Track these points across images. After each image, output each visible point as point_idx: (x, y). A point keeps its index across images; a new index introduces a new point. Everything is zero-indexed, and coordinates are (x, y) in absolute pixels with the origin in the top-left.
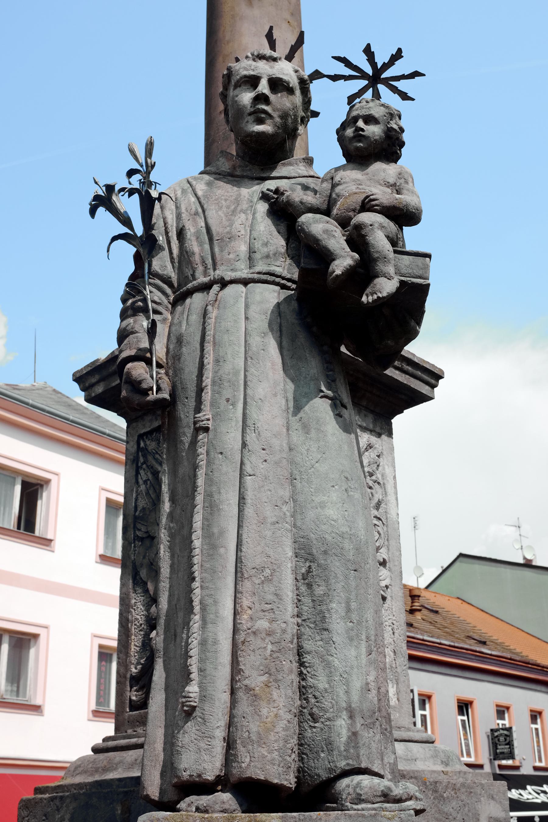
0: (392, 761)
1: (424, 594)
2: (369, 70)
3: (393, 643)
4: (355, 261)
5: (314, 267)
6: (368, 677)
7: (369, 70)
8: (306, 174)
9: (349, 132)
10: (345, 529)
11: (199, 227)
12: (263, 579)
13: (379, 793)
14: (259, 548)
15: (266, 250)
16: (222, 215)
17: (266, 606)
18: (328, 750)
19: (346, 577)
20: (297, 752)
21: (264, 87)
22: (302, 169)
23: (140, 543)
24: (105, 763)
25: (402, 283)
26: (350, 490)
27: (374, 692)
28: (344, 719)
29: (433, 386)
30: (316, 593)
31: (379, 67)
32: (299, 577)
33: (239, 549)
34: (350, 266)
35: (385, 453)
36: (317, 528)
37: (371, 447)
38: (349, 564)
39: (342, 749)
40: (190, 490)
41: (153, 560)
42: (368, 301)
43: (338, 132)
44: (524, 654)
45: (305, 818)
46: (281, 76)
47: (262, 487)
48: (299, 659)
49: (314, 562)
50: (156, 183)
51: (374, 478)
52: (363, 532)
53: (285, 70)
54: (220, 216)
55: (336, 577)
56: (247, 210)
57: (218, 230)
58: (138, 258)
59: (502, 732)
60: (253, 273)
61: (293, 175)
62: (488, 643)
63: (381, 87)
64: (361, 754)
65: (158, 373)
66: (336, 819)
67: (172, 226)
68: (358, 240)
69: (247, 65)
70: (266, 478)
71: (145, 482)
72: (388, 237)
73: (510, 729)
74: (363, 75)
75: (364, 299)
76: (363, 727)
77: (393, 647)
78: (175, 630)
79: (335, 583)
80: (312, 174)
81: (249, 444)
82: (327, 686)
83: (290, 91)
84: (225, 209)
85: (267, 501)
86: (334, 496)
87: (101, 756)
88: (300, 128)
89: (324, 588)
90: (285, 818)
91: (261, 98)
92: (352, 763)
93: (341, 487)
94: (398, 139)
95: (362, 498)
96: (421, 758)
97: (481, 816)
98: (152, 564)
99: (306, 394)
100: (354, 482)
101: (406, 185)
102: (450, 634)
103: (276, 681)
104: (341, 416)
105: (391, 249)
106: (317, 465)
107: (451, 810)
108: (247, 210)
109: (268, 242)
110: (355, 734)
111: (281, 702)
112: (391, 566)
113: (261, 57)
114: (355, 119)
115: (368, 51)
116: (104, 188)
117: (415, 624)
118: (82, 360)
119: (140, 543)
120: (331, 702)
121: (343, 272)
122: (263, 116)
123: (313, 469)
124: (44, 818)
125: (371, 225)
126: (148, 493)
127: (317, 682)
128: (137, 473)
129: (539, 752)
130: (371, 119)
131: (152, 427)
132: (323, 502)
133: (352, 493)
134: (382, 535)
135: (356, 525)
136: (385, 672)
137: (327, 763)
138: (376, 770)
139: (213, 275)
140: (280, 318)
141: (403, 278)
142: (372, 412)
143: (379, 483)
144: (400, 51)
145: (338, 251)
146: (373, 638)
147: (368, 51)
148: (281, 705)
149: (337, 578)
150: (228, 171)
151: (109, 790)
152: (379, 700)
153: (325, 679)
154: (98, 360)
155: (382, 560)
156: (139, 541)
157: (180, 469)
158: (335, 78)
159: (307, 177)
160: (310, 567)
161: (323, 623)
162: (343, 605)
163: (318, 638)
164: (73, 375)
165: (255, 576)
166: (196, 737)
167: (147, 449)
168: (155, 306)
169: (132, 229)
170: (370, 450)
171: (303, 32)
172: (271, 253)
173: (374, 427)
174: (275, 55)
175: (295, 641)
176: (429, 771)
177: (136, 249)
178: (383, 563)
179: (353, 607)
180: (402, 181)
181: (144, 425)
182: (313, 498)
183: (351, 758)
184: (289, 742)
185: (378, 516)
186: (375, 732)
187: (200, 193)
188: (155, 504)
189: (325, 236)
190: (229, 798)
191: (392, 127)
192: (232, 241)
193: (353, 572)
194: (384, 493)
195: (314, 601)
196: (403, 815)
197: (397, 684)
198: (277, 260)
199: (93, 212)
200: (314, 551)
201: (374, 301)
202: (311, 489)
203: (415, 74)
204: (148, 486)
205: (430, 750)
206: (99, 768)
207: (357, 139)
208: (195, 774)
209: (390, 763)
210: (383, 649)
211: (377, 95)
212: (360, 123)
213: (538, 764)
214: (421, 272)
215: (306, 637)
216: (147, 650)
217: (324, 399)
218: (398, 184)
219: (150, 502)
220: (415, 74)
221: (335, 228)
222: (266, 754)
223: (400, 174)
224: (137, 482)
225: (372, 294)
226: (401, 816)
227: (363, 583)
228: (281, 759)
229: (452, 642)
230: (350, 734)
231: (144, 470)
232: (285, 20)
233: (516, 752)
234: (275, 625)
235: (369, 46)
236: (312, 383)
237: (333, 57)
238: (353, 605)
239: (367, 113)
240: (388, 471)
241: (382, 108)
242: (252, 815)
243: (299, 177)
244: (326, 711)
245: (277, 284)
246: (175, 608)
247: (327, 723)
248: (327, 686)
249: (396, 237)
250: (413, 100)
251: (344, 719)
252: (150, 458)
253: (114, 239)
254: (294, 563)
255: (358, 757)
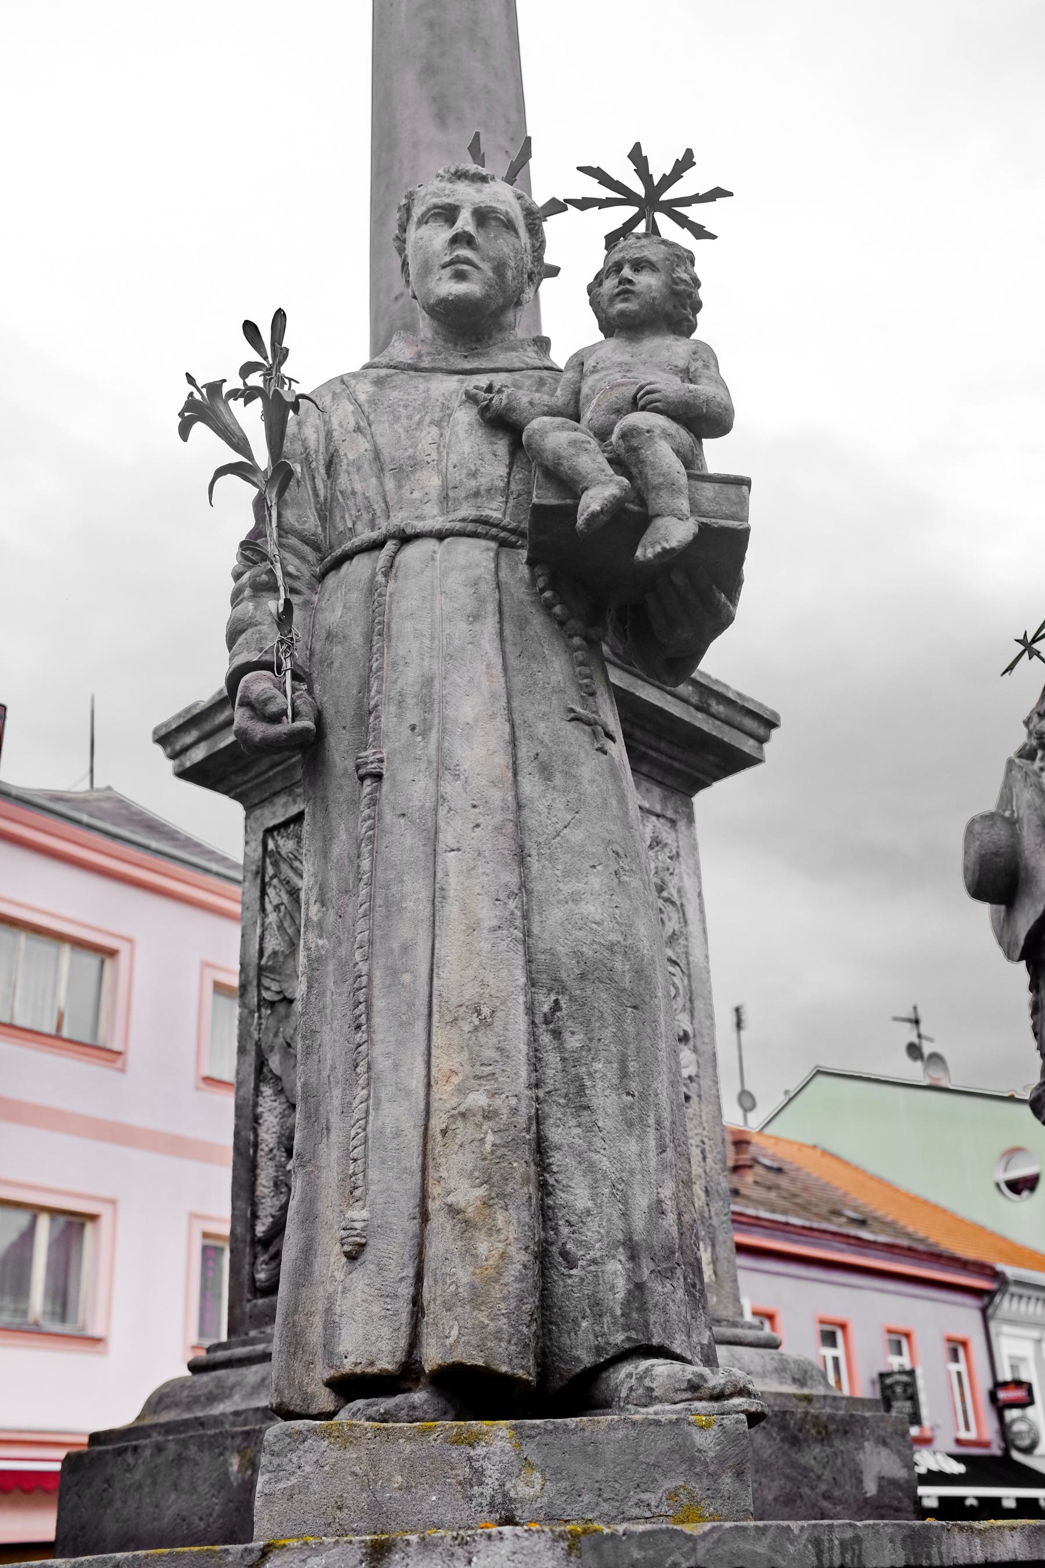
0: (706, 1342)
1: (755, 1139)
2: (638, 188)
3: (703, 1176)
4: (623, 489)
5: (554, 502)
6: (660, 1190)
7: (638, 188)
8: (539, 363)
9: (610, 284)
10: (614, 937)
11: (363, 450)
12: (477, 1023)
13: (684, 1385)
14: (470, 972)
15: (473, 483)
16: (401, 430)
17: (483, 1068)
18: (594, 1316)
19: (619, 1018)
20: (539, 1322)
21: (465, 222)
22: (531, 356)
23: (269, 1012)
24: (211, 1386)
25: (703, 528)
26: (622, 873)
27: (671, 1218)
28: (620, 1261)
29: (762, 740)
30: (568, 1046)
31: (656, 183)
32: (539, 1019)
33: (435, 975)
34: (615, 497)
35: (682, 853)
36: (567, 936)
37: (658, 843)
38: (624, 997)
39: (619, 1312)
40: (351, 881)
41: (291, 1038)
42: (645, 556)
43: (590, 290)
44: (932, 1240)
45: (556, 1428)
46: (494, 205)
47: (474, 868)
48: (541, 1160)
49: (563, 993)
50: (290, 380)
51: (665, 894)
52: (646, 944)
53: (499, 195)
54: (396, 431)
55: (601, 1017)
56: (441, 420)
57: (393, 453)
58: (260, 505)
59: (898, 1377)
60: (453, 521)
61: (517, 365)
62: (869, 1222)
63: (660, 218)
64: (651, 1321)
65: (294, 690)
66: (609, 1428)
67: (316, 452)
68: (626, 461)
69: (438, 189)
70: (479, 855)
71: (277, 908)
72: (678, 453)
73: (911, 1373)
74: (629, 197)
75: (639, 553)
76: (653, 1276)
77: (703, 1182)
78: (328, 1120)
79: (600, 1028)
80: (548, 364)
81: (449, 798)
82: (590, 1204)
83: (509, 225)
84: (404, 421)
85: (481, 891)
86: (596, 882)
87: (205, 1378)
88: (527, 290)
89: (581, 1036)
90: (521, 1427)
91: (461, 239)
92: (635, 1337)
93: (607, 867)
94: (690, 296)
95: (645, 888)
96: (757, 1373)
97: (865, 1474)
98: (289, 1045)
99: (544, 714)
100: (629, 860)
101: (705, 371)
102: (805, 1208)
103: (502, 1196)
104: (605, 753)
105: (683, 470)
106: (566, 831)
107: (812, 1462)
108: (441, 420)
109: (477, 470)
110: (640, 1287)
111: (512, 1232)
112: (698, 1044)
113: (460, 175)
114: (618, 267)
115: (637, 157)
116: (204, 391)
117: (743, 1191)
118: (169, 710)
119: (269, 1012)
120: (598, 1232)
121: (602, 509)
122: (465, 267)
123: (559, 838)
124: (106, 1486)
125: (648, 432)
126: (281, 927)
127: (573, 1198)
128: (263, 893)
129: (965, 1412)
130: (644, 264)
131: (287, 816)
132: (578, 893)
133: (626, 879)
134: (681, 991)
135: (635, 932)
136: (690, 1188)
137: (591, 1337)
138: (678, 1351)
139: (384, 526)
140: (500, 592)
141: (704, 520)
142: (659, 783)
143: (673, 903)
144: (689, 153)
145: (594, 474)
146: (667, 1124)
147: (637, 157)
148: (511, 1237)
149: (604, 1019)
150: (409, 361)
151: (217, 1431)
152: (682, 1234)
153: (587, 1192)
154: (197, 704)
155: (682, 1034)
156: (266, 1008)
157: (334, 846)
158: (584, 204)
159: (540, 368)
160: (556, 1001)
161: (581, 1096)
162: (615, 1065)
163: (572, 1122)
164: (155, 733)
165: (463, 1019)
166: (364, 1297)
167: (279, 853)
168: (289, 581)
169: (250, 456)
170: (657, 848)
171: (530, 138)
172: (482, 488)
173: (663, 809)
174: (484, 171)
175: (534, 1128)
176: (771, 1394)
177: (257, 490)
178: (684, 1038)
179: (632, 1069)
180: (699, 364)
181: (274, 813)
182: (561, 885)
183: (634, 1329)
184: (525, 1301)
185: (674, 958)
186: (675, 1284)
187: (362, 398)
188: (294, 945)
189: (572, 451)
190: (423, 1399)
191: (679, 278)
192: (416, 470)
193: (630, 1010)
194: (682, 920)
195: (566, 1059)
196: (728, 1421)
197: (713, 1246)
198: (493, 499)
199: (184, 432)
200: (564, 975)
201: (658, 556)
202: (557, 872)
203: (717, 193)
204: (281, 914)
205: (772, 1359)
206: (199, 1397)
207: (621, 297)
208: (364, 1361)
209: (702, 1345)
210: (685, 1147)
211: (653, 229)
212: (627, 272)
213: (963, 1435)
214: (734, 509)
215: (552, 1121)
216: (281, 1193)
217: (573, 723)
218: (692, 369)
219: (285, 941)
220: (717, 193)
221: (589, 439)
222: (487, 1322)
223: (695, 353)
224: (263, 909)
225: (653, 545)
226: (724, 1422)
227: (649, 1030)
228: (512, 1331)
229: (809, 1220)
230: (632, 1286)
231: (275, 887)
232: (501, 148)
233: (925, 1412)
234: (498, 1102)
235: (638, 146)
236: (555, 696)
237: (578, 168)
238: (633, 1066)
239: (637, 256)
240: (688, 883)
241: (662, 247)
242: (462, 1423)
243: (528, 369)
244: (589, 1247)
245: (493, 538)
246: (327, 1082)
247: (592, 1268)
248: (590, 1204)
249: (690, 454)
250: (714, 237)
251: (620, 1261)
252: (284, 867)
253: (221, 472)
254: (529, 996)
255: (646, 1325)
